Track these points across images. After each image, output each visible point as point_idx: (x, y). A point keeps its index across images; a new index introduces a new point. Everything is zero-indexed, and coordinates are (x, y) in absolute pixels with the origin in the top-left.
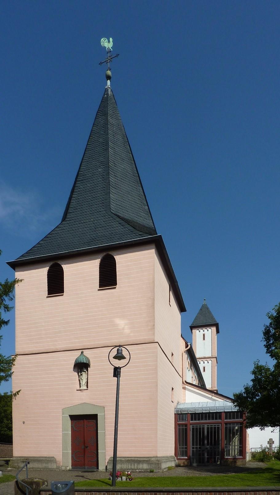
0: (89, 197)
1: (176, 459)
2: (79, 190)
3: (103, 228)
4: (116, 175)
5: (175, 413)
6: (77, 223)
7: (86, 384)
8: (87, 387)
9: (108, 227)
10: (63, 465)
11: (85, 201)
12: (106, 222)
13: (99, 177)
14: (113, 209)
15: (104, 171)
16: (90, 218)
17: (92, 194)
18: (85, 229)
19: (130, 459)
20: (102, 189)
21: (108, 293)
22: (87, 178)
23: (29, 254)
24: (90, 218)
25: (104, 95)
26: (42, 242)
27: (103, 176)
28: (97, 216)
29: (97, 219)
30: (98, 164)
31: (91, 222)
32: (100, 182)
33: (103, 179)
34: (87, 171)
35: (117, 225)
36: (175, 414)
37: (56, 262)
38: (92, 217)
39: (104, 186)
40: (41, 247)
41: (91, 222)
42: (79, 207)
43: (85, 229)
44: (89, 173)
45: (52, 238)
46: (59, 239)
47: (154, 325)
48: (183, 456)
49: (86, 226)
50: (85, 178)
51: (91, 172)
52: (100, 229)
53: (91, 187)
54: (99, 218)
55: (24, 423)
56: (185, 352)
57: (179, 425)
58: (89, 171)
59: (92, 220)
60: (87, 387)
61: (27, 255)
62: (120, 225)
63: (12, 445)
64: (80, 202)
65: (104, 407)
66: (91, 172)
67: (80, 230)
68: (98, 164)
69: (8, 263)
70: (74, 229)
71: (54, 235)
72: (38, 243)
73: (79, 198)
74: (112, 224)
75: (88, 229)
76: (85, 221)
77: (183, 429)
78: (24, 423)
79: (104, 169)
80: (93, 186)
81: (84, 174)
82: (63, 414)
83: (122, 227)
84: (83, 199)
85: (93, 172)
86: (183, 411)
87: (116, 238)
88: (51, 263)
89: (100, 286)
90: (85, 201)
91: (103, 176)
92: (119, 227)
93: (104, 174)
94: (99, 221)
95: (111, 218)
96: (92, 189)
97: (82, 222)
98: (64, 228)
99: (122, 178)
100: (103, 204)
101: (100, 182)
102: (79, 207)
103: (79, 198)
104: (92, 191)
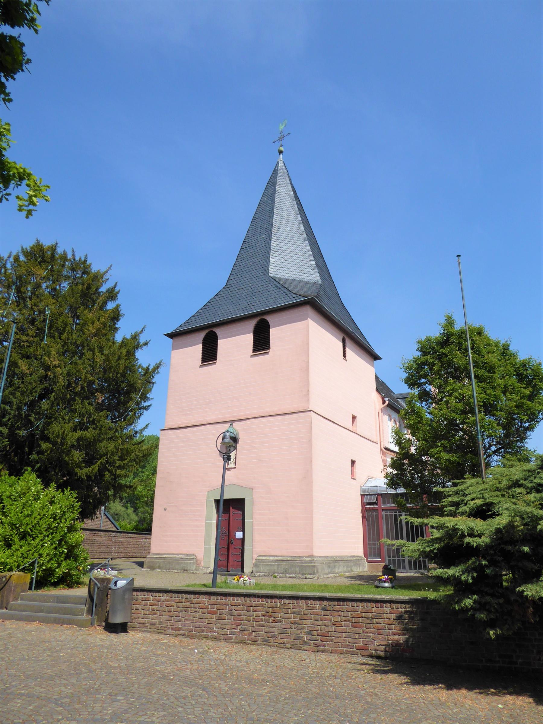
0: (251, 263)
1: (366, 561)
2: (242, 257)
3: (259, 293)
4: (279, 238)
5: (362, 493)
6: (236, 289)
7: (234, 461)
8: (235, 465)
9: (264, 291)
10: (204, 566)
11: (246, 267)
12: (263, 287)
13: (261, 243)
14: (272, 273)
15: (267, 237)
16: (248, 283)
17: (253, 260)
18: (243, 295)
19: (280, 558)
20: (263, 254)
21: (262, 359)
22: (251, 245)
23: (187, 324)
24: (248, 283)
25: (275, 167)
26: (201, 311)
27: (266, 242)
28: (256, 281)
29: (255, 284)
30: (262, 231)
31: (249, 288)
32: (262, 248)
33: (265, 245)
34: (251, 239)
35: (274, 289)
36: (361, 495)
37: (212, 330)
38: (251, 282)
39: (266, 251)
40: (199, 316)
41: (249, 288)
42: (240, 273)
43: (243, 295)
44: (253, 240)
45: (210, 306)
46: (217, 306)
47: (308, 391)
48: (375, 556)
49: (244, 292)
50: (249, 245)
51: (255, 239)
52: (257, 293)
53: (253, 253)
54: (257, 283)
55: (165, 510)
56: (382, 409)
57: (367, 510)
58: (253, 238)
59: (250, 285)
60: (235, 465)
61: (185, 324)
62: (276, 288)
63: (151, 535)
64: (242, 268)
65: (253, 489)
66: (255, 239)
67: (238, 296)
68: (262, 231)
69: (165, 335)
70: (232, 295)
71: (212, 303)
72: (197, 313)
73: (241, 264)
74: (269, 287)
75: (245, 294)
76: (243, 287)
77: (391, 515)
78: (165, 510)
79: (267, 235)
80: (255, 252)
81: (248, 242)
82: (208, 498)
83: (278, 290)
84: (244, 265)
85: (257, 239)
86: (372, 491)
87: (270, 302)
88: (206, 332)
89: (254, 351)
90: (246, 267)
91: (266, 242)
92: (275, 291)
93: (267, 240)
94: (257, 286)
95: (269, 282)
96: (254, 255)
97: (241, 288)
98: (223, 295)
99: (286, 240)
100: (262, 269)
101: (262, 248)
102: (240, 273)
103: (241, 264)
104: (253, 257)
